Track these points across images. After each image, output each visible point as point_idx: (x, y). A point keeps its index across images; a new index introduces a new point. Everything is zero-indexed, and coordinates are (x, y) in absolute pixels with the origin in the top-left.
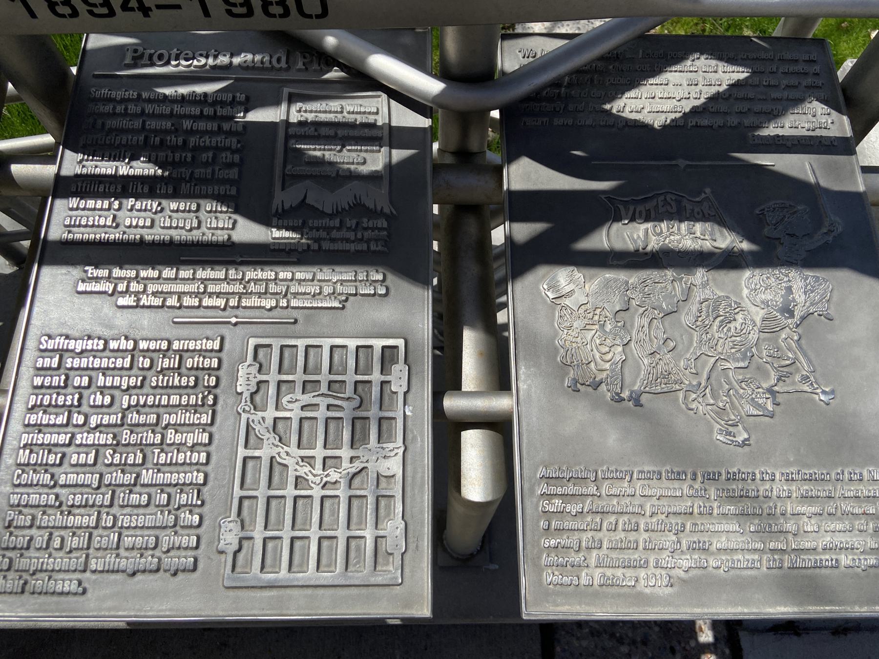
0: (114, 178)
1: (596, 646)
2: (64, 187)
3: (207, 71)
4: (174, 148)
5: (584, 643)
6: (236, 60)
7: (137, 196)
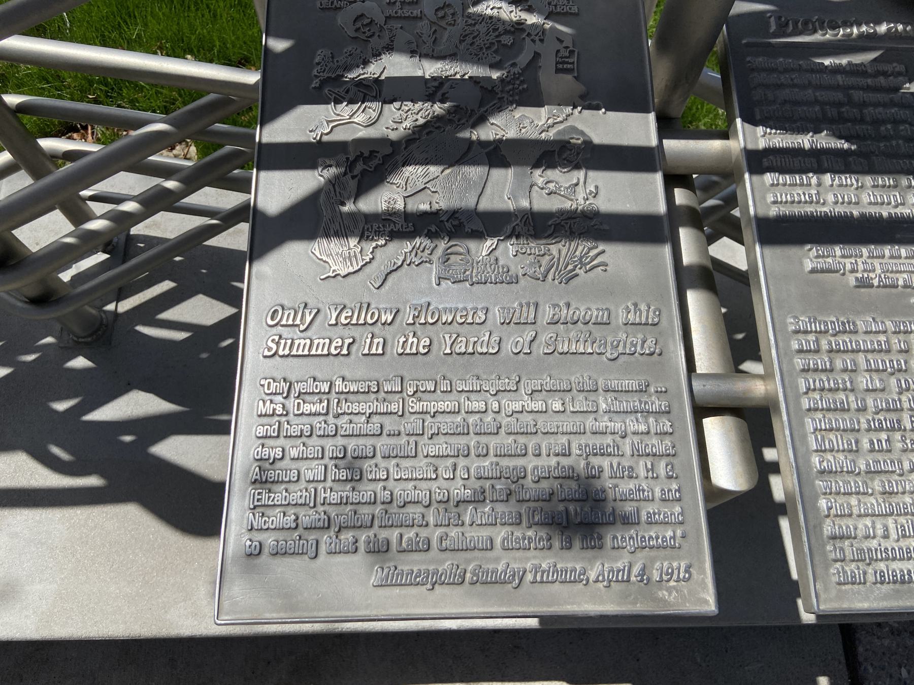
0: (798, 152)
1: (898, 645)
2: (759, 161)
3: (854, 40)
4: (854, 121)
5: (886, 642)
6: (883, 28)
7: (834, 171)
